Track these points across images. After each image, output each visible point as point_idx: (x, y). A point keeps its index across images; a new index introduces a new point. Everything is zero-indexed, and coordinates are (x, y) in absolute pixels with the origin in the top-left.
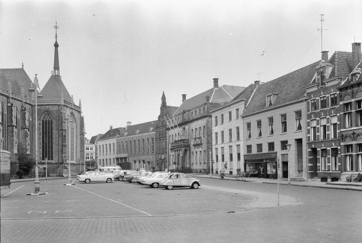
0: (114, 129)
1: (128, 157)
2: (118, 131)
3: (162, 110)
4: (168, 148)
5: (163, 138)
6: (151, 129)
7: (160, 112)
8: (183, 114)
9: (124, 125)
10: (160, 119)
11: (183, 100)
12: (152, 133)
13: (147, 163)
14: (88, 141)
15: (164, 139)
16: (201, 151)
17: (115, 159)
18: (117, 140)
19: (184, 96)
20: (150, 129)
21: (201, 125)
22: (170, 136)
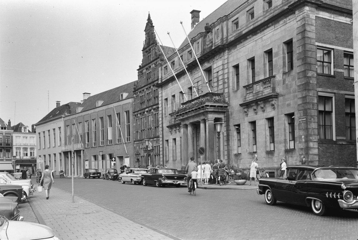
0: (62, 106)
1: (83, 150)
2: (67, 107)
3: (146, 52)
4: (161, 126)
5: (150, 108)
6: (125, 95)
7: (141, 58)
8: (205, 36)
9: (79, 99)
10: (141, 72)
11: (193, 23)
12: (128, 101)
13: (117, 159)
14: (25, 128)
15: (151, 110)
16: (271, 120)
17: (62, 153)
18: (65, 121)
19: (195, 14)
20: (122, 95)
21: (271, 43)
22: (166, 99)
